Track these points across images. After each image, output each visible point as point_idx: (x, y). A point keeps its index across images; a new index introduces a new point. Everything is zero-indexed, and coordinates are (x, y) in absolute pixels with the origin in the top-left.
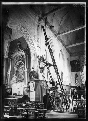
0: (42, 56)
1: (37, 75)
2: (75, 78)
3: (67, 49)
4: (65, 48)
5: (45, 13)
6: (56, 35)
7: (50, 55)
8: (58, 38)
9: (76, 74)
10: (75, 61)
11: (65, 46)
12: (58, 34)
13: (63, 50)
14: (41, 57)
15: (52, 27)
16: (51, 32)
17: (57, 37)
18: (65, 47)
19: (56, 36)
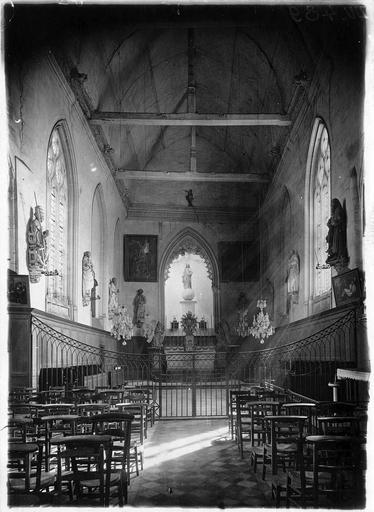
0: (37, 207)
1: (21, 288)
2: (133, 307)
3: (118, 183)
4: (112, 178)
5: (105, 109)
6: (89, 114)
7: (7, 232)
8: (92, 129)
9: (140, 292)
10: (142, 238)
11: (115, 171)
12: (97, 111)
13: (104, 187)
14: (32, 209)
15: (80, 76)
16: (72, 98)
17: (91, 125)
18: (114, 175)
19: (89, 119)
